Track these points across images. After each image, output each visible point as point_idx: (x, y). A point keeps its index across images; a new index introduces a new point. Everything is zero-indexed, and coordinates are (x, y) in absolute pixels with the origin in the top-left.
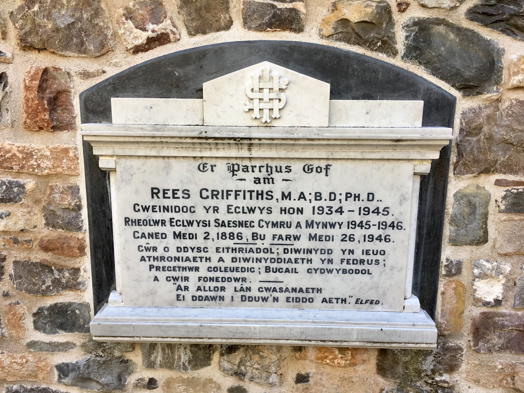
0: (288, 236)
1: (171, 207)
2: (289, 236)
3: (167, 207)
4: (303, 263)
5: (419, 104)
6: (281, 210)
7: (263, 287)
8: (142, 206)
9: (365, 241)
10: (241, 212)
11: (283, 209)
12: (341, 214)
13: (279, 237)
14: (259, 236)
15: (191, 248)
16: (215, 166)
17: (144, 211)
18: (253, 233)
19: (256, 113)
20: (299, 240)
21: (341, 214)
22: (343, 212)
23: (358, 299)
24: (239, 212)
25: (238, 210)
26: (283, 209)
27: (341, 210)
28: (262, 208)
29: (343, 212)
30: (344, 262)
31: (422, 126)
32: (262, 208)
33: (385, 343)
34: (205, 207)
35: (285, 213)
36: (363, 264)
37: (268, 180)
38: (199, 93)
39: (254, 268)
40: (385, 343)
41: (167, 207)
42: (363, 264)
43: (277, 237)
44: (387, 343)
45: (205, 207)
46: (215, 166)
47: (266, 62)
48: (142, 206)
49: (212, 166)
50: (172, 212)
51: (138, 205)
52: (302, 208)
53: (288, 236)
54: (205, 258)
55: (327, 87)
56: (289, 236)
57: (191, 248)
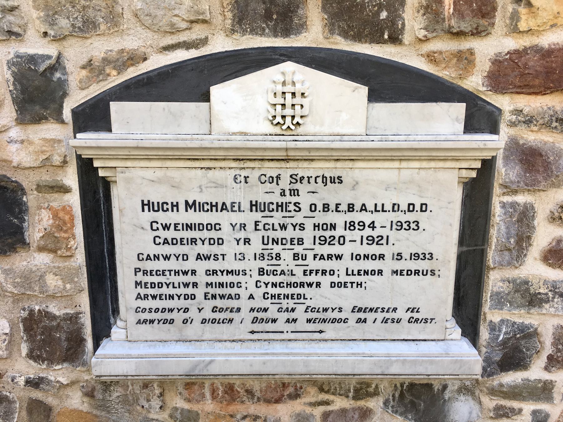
0: (193, 240)
1: (195, 224)
2: (195, 240)
3: (190, 225)
4: (352, 287)
5: (460, 109)
6: (315, 226)
7: (235, 301)
8: (162, 224)
9: (411, 259)
10: (271, 229)
11: (317, 224)
12: (373, 230)
13: (321, 257)
14: (300, 256)
15: (220, 271)
16: (248, 177)
17: (164, 230)
18: (294, 254)
19: (279, 119)
20: (340, 259)
21: (373, 230)
22: (376, 227)
23: (308, 307)
24: (269, 229)
25: (267, 227)
26: (317, 224)
27: (373, 225)
28: (294, 225)
29: (376, 227)
30: (312, 273)
31: (464, 133)
32: (294, 225)
33: (439, 375)
34: (231, 224)
35: (319, 230)
36: (325, 275)
37: (295, 192)
38: (206, 98)
39: (240, 283)
40: (439, 375)
41: (190, 225)
42: (325, 275)
43: (318, 257)
44: (441, 375)
45: (231, 224)
46: (248, 177)
47: (289, 62)
48: (162, 224)
49: (246, 178)
50: (195, 230)
51: (157, 223)
52: (335, 224)
53: (193, 240)
54: (174, 271)
55: (364, 90)
56: (195, 240)
57: (220, 271)
